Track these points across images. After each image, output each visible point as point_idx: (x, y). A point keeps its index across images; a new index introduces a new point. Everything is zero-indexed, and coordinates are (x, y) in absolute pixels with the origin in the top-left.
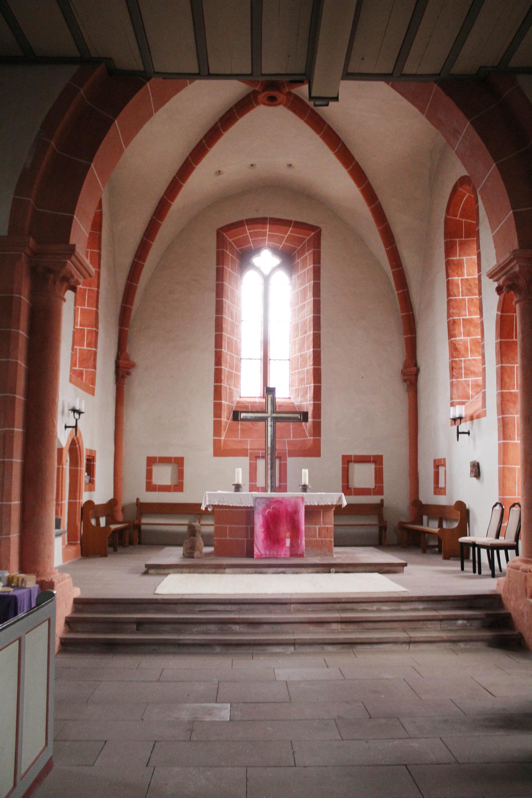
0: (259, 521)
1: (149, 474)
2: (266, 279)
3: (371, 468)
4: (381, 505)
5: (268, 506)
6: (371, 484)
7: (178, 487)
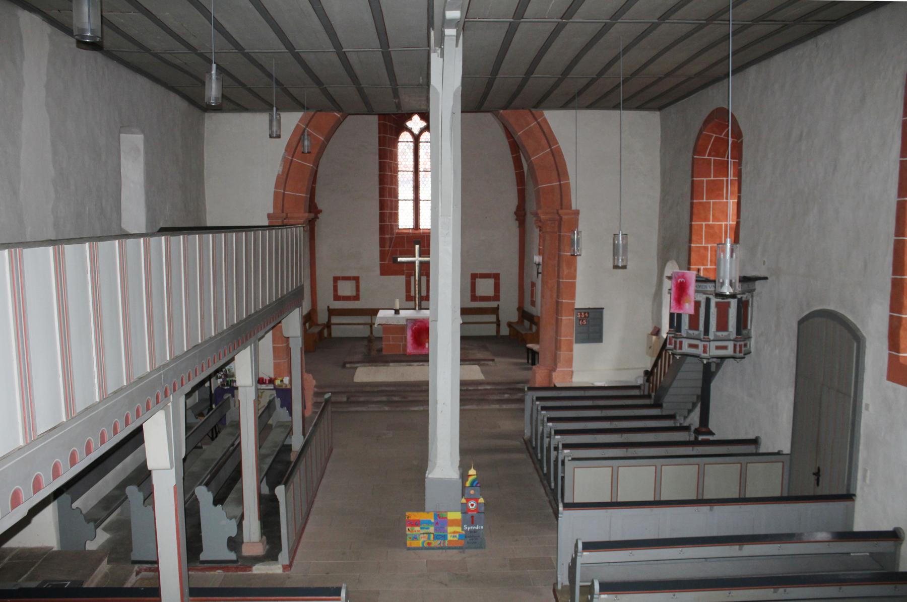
0: (409, 334)
1: (335, 289)
2: (416, 139)
3: (491, 281)
4: (498, 308)
5: (415, 324)
6: (491, 293)
7: (357, 298)
